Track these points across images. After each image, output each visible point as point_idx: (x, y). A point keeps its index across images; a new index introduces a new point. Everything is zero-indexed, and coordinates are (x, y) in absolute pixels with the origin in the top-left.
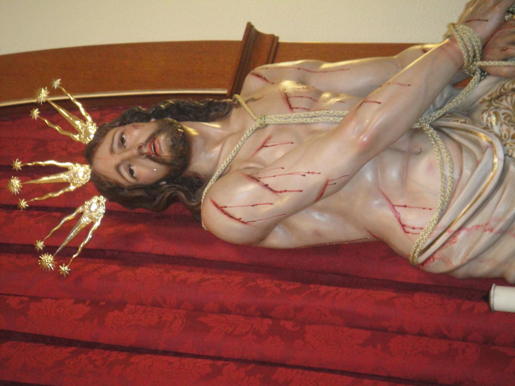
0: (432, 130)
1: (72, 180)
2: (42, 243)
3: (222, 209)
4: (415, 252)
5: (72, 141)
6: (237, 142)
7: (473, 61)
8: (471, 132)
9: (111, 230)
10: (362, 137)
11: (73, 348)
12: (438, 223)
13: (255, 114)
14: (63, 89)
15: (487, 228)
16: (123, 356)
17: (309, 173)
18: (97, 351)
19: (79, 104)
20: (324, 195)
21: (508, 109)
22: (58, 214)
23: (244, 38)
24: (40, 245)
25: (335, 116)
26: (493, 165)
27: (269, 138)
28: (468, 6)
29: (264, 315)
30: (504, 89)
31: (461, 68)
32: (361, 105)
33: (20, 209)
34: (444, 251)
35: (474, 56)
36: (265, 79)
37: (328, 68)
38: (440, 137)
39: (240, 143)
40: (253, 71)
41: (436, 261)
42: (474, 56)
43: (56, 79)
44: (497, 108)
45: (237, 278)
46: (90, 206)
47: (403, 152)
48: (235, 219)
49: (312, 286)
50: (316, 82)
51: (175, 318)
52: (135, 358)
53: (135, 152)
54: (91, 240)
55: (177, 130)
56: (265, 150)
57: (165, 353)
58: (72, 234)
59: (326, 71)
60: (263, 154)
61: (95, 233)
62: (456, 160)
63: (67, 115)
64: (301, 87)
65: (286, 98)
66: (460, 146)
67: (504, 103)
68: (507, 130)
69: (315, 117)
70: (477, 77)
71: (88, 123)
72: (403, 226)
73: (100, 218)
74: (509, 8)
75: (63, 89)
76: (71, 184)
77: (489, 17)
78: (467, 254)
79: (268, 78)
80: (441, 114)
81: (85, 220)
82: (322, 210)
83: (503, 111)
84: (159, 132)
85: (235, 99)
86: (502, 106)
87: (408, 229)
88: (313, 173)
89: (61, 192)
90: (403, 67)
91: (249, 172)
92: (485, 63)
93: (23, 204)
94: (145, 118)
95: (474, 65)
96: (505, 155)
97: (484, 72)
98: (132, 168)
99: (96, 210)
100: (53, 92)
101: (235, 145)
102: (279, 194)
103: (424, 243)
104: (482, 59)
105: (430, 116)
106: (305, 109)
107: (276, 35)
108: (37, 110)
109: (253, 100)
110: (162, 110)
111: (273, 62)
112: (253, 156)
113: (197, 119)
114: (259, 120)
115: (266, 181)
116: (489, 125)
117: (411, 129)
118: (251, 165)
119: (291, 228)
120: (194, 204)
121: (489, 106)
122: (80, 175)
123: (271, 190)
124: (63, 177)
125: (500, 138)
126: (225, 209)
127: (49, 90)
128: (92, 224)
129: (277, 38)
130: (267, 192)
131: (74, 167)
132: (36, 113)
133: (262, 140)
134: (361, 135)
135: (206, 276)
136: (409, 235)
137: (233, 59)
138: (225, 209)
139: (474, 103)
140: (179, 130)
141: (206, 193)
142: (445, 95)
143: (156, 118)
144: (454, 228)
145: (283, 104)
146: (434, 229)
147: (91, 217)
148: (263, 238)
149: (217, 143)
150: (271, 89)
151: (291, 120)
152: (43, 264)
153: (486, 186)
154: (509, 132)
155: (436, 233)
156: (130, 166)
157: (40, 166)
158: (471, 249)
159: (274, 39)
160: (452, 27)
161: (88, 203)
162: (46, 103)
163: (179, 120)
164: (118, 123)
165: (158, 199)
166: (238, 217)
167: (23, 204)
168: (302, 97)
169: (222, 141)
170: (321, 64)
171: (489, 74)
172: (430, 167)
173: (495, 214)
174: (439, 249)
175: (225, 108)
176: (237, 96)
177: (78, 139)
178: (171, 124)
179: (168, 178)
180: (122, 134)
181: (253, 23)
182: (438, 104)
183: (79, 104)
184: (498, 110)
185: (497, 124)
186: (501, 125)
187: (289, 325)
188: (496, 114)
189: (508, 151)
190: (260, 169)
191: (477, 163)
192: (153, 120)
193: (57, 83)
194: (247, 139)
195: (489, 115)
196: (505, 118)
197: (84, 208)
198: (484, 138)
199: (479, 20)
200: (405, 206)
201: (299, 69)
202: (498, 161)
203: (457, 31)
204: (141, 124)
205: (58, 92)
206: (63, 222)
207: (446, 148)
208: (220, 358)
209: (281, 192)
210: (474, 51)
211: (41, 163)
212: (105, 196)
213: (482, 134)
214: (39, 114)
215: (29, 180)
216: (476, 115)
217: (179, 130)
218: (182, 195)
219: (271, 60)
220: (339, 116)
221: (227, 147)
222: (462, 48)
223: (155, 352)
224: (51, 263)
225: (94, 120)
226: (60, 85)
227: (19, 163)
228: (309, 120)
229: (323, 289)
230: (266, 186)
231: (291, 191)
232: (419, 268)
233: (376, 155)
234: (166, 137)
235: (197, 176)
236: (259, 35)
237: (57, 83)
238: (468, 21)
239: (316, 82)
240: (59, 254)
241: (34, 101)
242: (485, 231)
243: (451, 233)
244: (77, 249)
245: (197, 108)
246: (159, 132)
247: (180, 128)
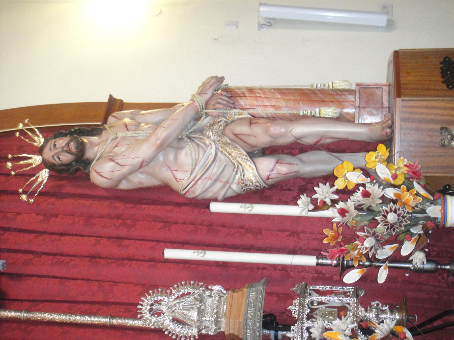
0: (187, 138)
1: (34, 162)
2: (21, 190)
3: (98, 173)
4: (181, 189)
5: (34, 146)
6: (105, 145)
7: (202, 110)
8: (202, 139)
9: (52, 184)
10: (157, 142)
11: (36, 234)
12: (190, 177)
13: (112, 133)
14: (30, 124)
15: (210, 178)
16: (58, 237)
17: (135, 157)
18: (46, 235)
19: (36, 130)
20: (142, 166)
21: (216, 129)
22: (28, 177)
23: (108, 101)
24: (21, 190)
25: (146, 133)
26: (211, 152)
27: (119, 143)
28: (200, 88)
29: (118, 218)
30: (215, 122)
31: (197, 113)
32: (156, 128)
33: (11, 175)
34: (193, 189)
35: (203, 108)
36: (117, 118)
37: (144, 113)
38: (190, 141)
39: (106, 145)
40: (111, 115)
41: (190, 193)
42: (203, 108)
43: (26, 119)
44: (212, 129)
45: (107, 203)
46: (42, 174)
47: (174, 148)
48: (105, 177)
49: (139, 205)
50: (138, 119)
51: (80, 220)
52: (63, 238)
53: (60, 150)
54: (42, 188)
55: (78, 140)
56: (117, 148)
57: (76, 235)
58: (34, 186)
59: (143, 114)
60: (116, 149)
61: (44, 185)
62: (196, 151)
63: (31, 135)
64: (132, 121)
65: (126, 126)
66: (198, 145)
67: (215, 127)
68: (217, 138)
69: (138, 133)
70: (204, 116)
71: (40, 138)
72: (176, 179)
73: (46, 179)
74: (216, 88)
75: (30, 124)
76: (34, 164)
77: (208, 92)
78: (202, 190)
79: (118, 118)
80: (190, 132)
81: (40, 180)
82: (142, 173)
83: (215, 130)
84: (71, 141)
85: (104, 127)
86: (214, 128)
87: (178, 180)
88: (137, 157)
89: (29, 168)
90: (175, 112)
91: (110, 157)
92: (207, 111)
93: (13, 173)
94: (65, 135)
95: (203, 112)
96: (216, 148)
97: (207, 115)
98: (59, 157)
99: (45, 175)
100: (25, 125)
101: (104, 146)
102: (123, 166)
103: (184, 185)
104: (206, 109)
105: (186, 133)
106: (134, 130)
107: (122, 99)
108: (18, 132)
109: (112, 127)
110: (72, 132)
111: (121, 110)
112: (112, 150)
113: (88, 135)
114: (114, 135)
115: (117, 161)
116: (210, 136)
117: (178, 138)
118: (111, 154)
119: (129, 181)
120: (87, 172)
121: (209, 128)
122: (37, 160)
123: (120, 165)
124: (30, 161)
125: (214, 141)
126: (100, 173)
127: (23, 124)
128: (43, 181)
129: (123, 101)
130: (118, 166)
131: (35, 157)
132: (18, 134)
133: (115, 144)
134: (157, 141)
135: (94, 202)
136: (178, 182)
137: (104, 109)
138: (100, 174)
139: (203, 127)
140: (80, 140)
141: (92, 167)
142: (192, 124)
143: (70, 135)
144: (197, 179)
145: (124, 128)
146: (188, 179)
147: (42, 178)
148: (117, 185)
149: (96, 145)
150: (119, 122)
151: (128, 135)
152: (22, 199)
153: (209, 161)
154: (217, 139)
155: (189, 181)
156: (58, 156)
157: (20, 157)
158: (203, 187)
159: (121, 101)
160: (193, 96)
161: (41, 172)
162: (22, 130)
163: (80, 136)
164: (53, 137)
165: (71, 169)
166: (106, 176)
167: (13, 173)
168: (132, 125)
169: (99, 144)
170: (141, 112)
171: (209, 115)
172: (186, 154)
173: (213, 173)
174: (191, 188)
175: (100, 131)
176: (105, 125)
177: (36, 145)
178: (76, 137)
179: (76, 161)
180: (55, 142)
181: (112, 95)
182: (189, 128)
183: (36, 130)
184: (213, 130)
185: (212, 136)
186: (214, 136)
187: (129, 222)
188: (212, 131)
189: (217, 147)
190: (115, 156)
191: (205, 152)
192: (68, 136)
193: (26, 121)
194: (109, 143)
195: (209, 132)
196: (215, 133)
197: (39, 174)
198: (207, 142)
199: (204, 93)
200: (177, 170)
201: (131, 113)
202: (213, 151)
203: (195, 98)
204: (63, 138)
205: (28, 125)
206: (30, 180)
207: (192, 146)
208: (100, 237)
209: (124, 166)
210: (202, 106)
211: (20, 155)
212: (48, 168)
213: (207, 140)
214: (19, 135)
215: (15, 163)
216: (204, 132)
217: (80, 140)
218: (82, 168)
219: (120, 110)
220: (148, 133)
221: (101, 147)
222: (197, 105)
223: (71, 235)
224: (26, 198)
225: (43, 136)
226: (28, 122)
227: (11, 155)
228: (135, 135)
229: (143, 206)
230: (117, 163)
231: (128, 165)
232: (183, 196)
233: (163, 149)
234: (74, 143)
235: (88, 159)
236: (115, 99)
237: (26, 121)
238: (200, 94)
239: (138, 119)
240: (29, 194)
241: (17, 129)
242: (209, 180)
243: (195, 182)
244: (37, 192)
245: (88, 131)
246: (71, 141)
247: (80, 139)
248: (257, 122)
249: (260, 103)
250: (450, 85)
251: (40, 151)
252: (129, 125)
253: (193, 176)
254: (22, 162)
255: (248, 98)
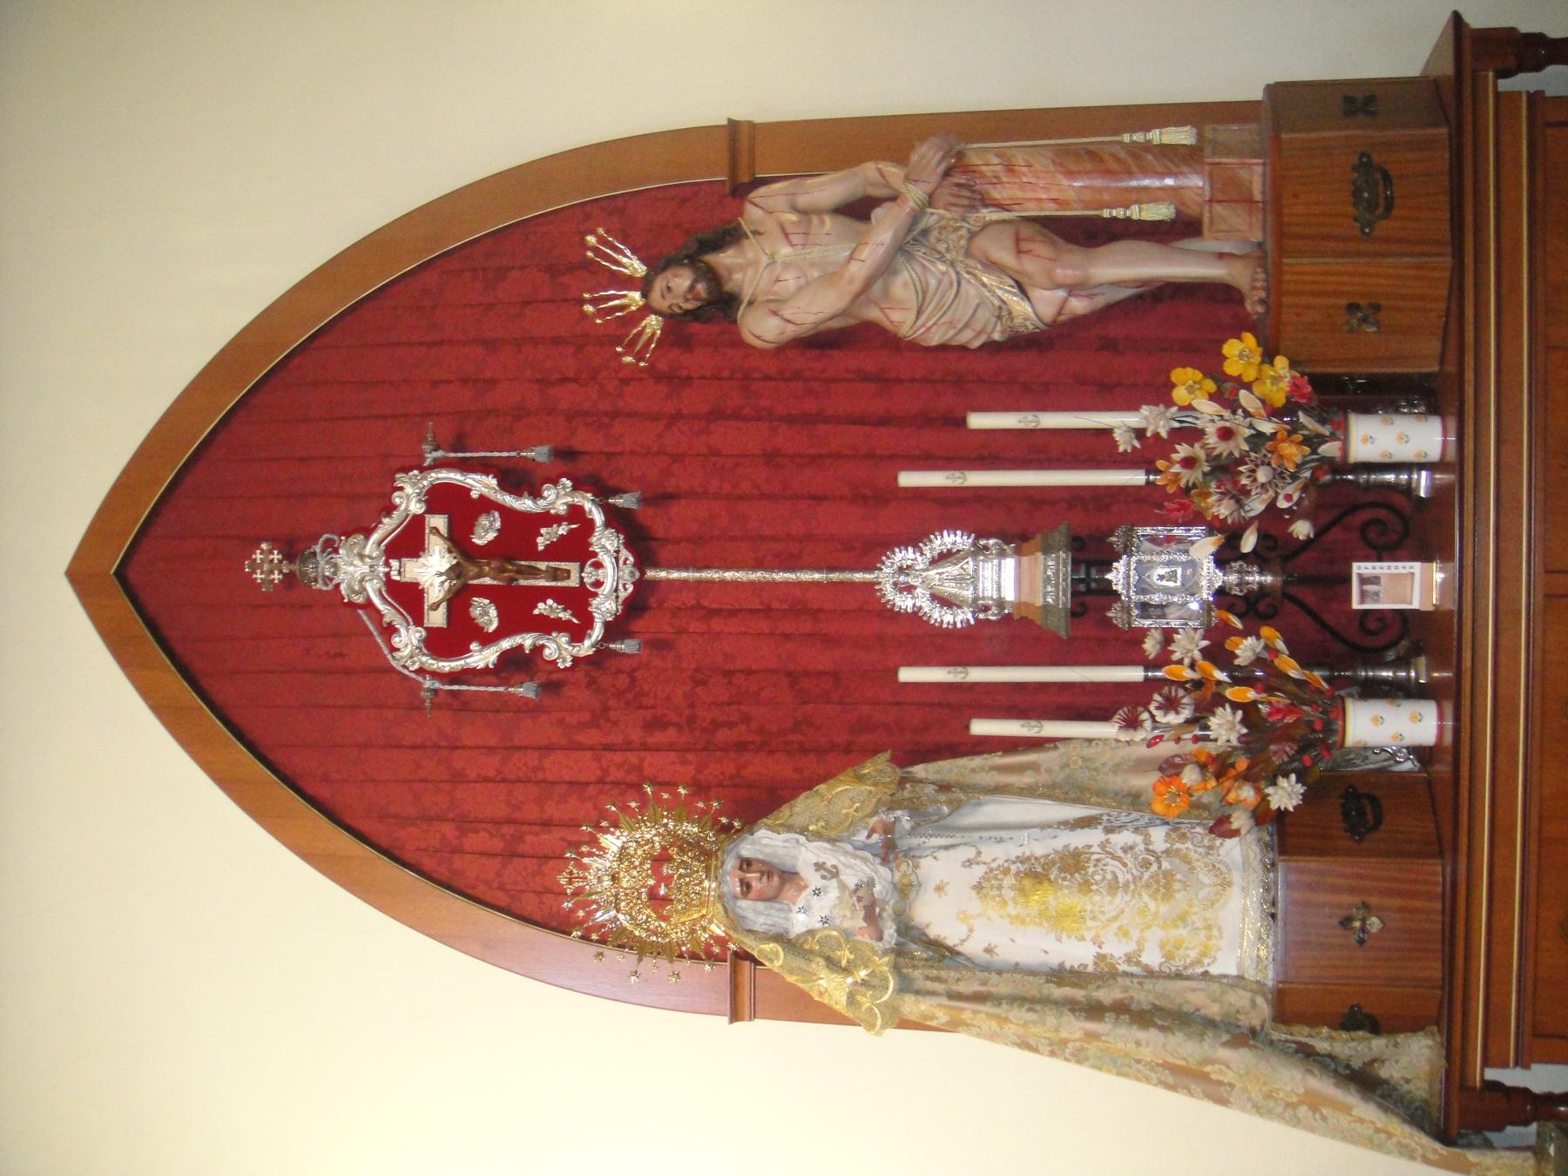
248: (1030, 251)
249: (1030, 195)
250: (1309, 542)
251: (647, 310)
252: (842, 498)
253: (920, 322)
254: (611, 303)
255: (1008, 185)
